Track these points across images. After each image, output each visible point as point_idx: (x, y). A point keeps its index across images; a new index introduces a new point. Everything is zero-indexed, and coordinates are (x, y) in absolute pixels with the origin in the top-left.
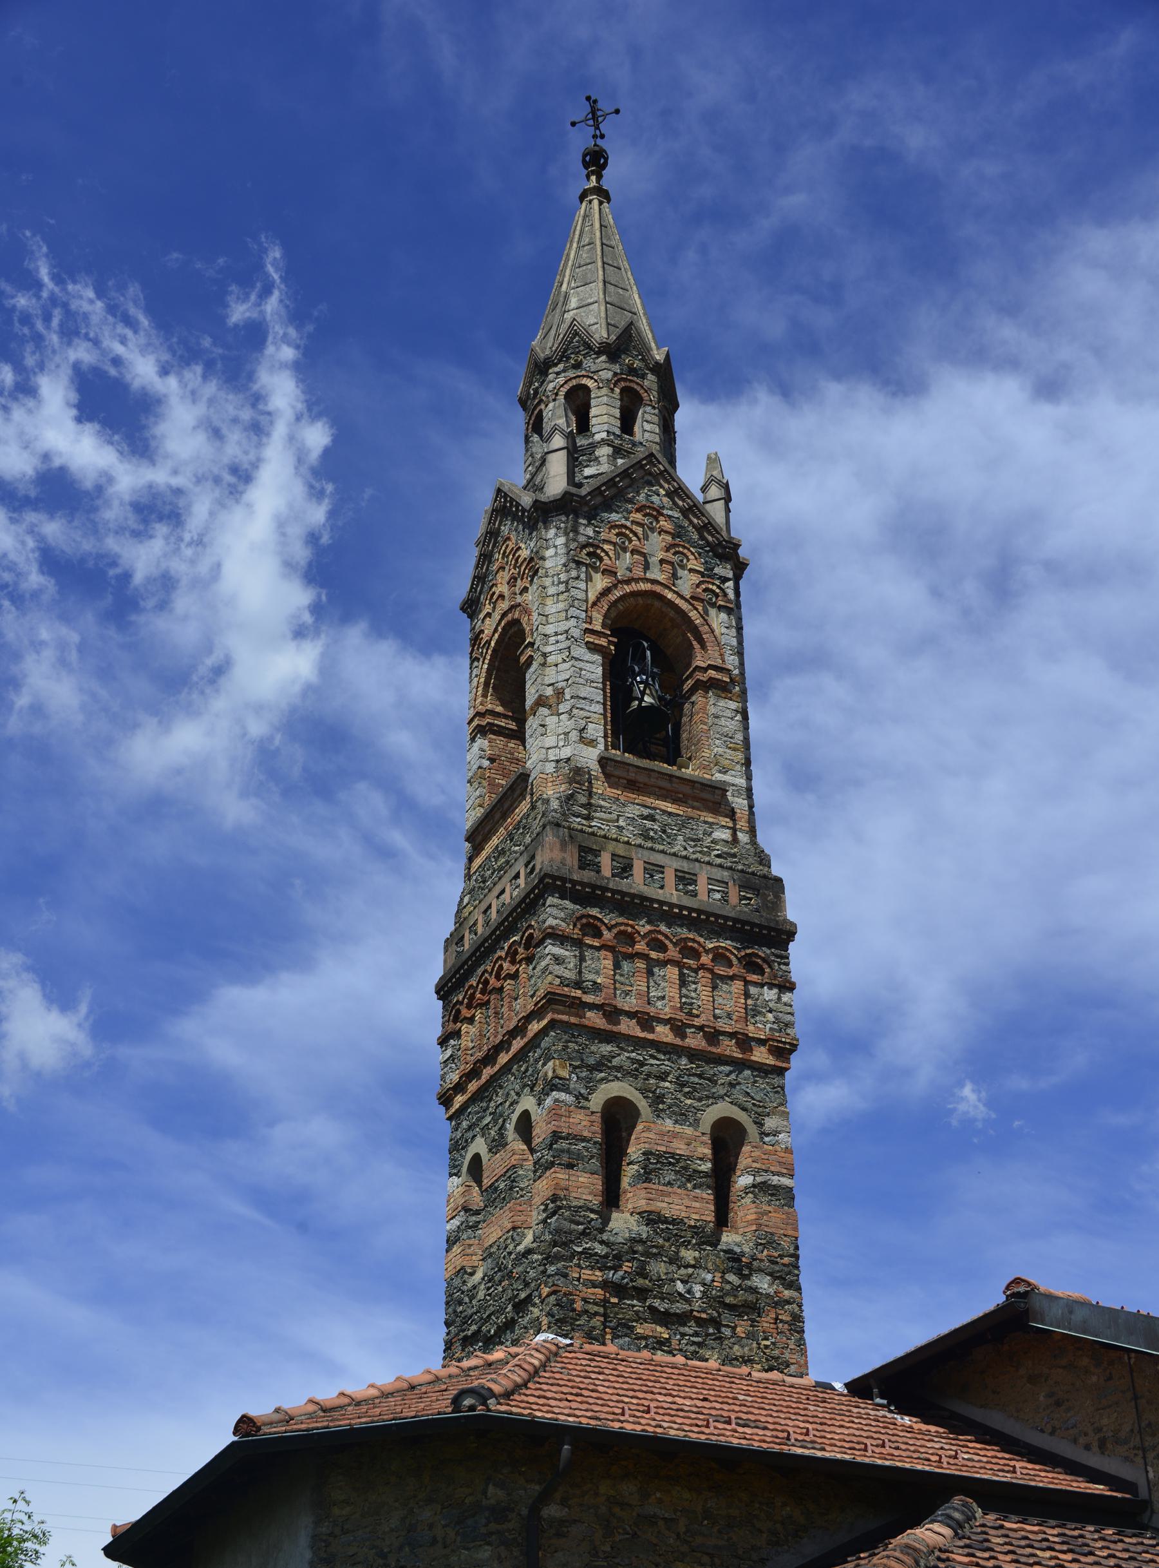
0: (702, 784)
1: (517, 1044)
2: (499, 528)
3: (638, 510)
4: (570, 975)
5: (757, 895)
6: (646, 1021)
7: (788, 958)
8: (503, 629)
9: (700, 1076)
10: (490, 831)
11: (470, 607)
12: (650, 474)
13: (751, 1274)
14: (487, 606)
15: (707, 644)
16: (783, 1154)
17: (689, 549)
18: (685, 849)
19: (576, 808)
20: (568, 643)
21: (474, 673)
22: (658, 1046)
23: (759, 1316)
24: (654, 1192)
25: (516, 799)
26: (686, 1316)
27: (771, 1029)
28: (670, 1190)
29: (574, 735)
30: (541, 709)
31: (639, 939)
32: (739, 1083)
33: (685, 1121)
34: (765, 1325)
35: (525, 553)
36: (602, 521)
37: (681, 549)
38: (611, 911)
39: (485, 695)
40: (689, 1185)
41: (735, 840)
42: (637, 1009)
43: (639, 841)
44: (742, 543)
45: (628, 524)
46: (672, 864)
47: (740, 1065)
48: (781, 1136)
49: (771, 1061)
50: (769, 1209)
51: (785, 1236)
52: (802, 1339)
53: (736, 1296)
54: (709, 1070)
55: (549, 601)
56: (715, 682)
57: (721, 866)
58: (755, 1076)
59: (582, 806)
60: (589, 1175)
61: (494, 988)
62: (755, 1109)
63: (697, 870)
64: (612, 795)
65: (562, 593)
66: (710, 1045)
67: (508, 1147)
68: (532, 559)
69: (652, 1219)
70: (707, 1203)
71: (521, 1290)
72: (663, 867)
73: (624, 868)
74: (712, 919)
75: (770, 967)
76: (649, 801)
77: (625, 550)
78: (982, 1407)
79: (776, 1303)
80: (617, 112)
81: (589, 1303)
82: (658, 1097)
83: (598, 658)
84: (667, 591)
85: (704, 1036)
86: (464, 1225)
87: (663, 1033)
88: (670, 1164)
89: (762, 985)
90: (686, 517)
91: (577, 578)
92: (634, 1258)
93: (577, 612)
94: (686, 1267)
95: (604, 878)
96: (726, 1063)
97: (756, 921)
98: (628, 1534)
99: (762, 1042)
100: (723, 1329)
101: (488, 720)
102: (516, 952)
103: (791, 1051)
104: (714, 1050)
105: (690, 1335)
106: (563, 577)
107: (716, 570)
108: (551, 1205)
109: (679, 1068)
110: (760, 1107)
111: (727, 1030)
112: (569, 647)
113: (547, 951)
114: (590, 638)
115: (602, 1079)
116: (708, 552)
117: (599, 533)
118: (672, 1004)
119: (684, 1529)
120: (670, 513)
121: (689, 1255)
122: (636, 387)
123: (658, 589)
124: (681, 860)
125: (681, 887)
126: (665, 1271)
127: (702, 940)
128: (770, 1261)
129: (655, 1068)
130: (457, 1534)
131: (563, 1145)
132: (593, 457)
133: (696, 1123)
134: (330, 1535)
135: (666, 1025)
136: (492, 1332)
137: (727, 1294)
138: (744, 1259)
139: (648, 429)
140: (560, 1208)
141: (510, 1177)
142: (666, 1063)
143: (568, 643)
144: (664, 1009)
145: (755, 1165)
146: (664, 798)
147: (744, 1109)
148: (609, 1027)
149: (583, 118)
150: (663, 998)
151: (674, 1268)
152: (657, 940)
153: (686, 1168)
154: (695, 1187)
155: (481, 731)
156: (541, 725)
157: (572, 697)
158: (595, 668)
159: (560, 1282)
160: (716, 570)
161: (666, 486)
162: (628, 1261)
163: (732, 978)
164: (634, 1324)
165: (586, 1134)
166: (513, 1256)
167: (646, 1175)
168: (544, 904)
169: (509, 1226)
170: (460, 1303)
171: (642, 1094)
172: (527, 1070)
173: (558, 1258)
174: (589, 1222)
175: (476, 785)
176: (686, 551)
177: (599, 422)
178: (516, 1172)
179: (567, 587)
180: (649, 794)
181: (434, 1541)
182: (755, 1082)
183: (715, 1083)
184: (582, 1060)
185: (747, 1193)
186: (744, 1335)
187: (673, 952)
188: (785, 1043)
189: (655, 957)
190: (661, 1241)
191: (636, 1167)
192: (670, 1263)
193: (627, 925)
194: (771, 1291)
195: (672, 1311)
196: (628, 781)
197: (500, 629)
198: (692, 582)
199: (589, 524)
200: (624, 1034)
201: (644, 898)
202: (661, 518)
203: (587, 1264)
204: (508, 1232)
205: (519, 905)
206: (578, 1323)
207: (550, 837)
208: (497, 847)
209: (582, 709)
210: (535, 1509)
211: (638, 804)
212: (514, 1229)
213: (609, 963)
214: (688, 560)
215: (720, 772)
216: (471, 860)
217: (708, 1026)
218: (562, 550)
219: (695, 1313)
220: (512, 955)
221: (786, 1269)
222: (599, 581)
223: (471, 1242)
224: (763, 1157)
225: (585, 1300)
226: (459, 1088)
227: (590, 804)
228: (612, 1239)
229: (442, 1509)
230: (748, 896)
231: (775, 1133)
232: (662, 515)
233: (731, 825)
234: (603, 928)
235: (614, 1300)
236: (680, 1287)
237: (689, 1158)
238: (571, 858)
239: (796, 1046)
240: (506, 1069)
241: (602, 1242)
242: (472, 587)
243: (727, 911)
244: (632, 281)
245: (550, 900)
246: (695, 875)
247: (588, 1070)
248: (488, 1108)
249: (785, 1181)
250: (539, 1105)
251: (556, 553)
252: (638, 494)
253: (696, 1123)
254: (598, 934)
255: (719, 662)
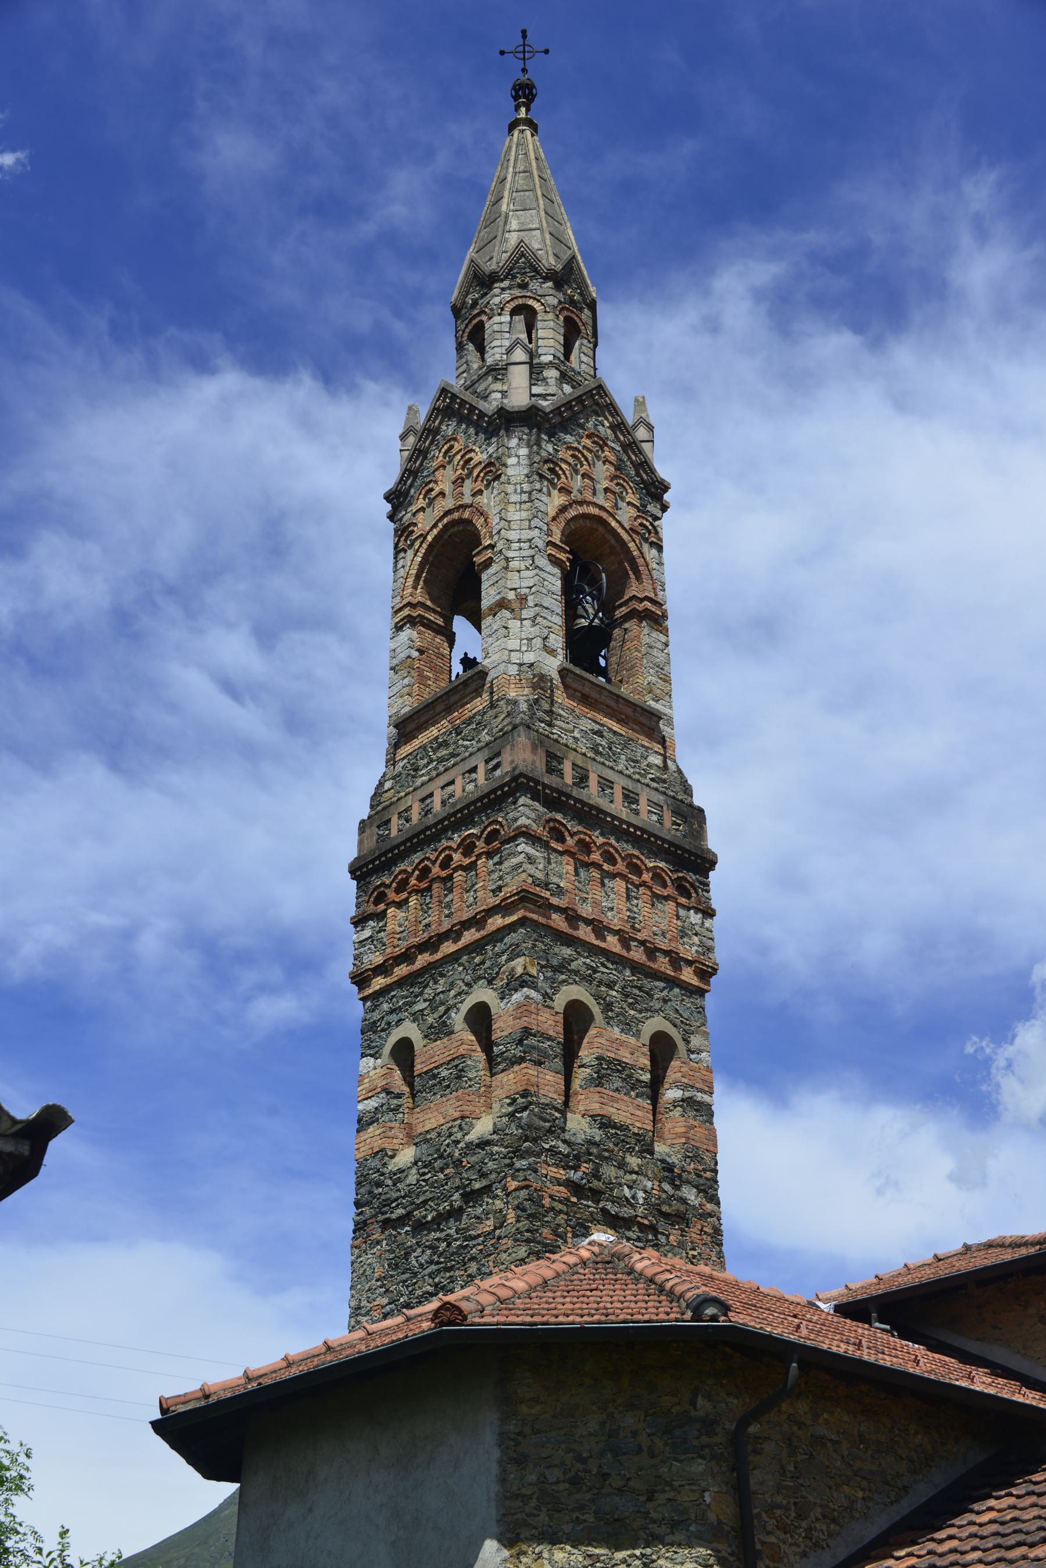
0: (643, 709)
1: (470, 936)
2: (439, 427)
3: (589, 437)
4: (540, 875)
5: (685, 822)
6: (600, 929)
7: (708, 886)
8: (445, 526)
9: (640, 989)
10: (426, 722)
11: (397, 498)
12: (597, 404)
13: (681, 1186)
14: (421, 500)
15: (643, 576)
16: (705, 1073)
17: (628, 483)
18: (627, 769)
19: (540, 714)
20: (532, 552)
21: (400, 565)
22: (606, 953)
23: (687, 1227)
24: (605, 1096)
25: (468, 695)
26: (631, 1221)
27: (697, 951)
28: (618, 1096)
29: (538, 643)
30: (504, 611)
31: (594, 849)
32: (670, 1000)
33: (630, 1030)
34: (693, 1235)
35: (480, 456)
36: (560, 441)
37: (622, 482)
38: (572, 819)
39: (415, 587)
40: (632, 1093)
41: (665, 767)
42: (594, 916)
43: (590, 754)
44: (672, 486)
45: (581, 448)
46: (620, 782)
47: (673, 982)
48: (704, 1054)
49: (695, 981)
50: (696, 1123)
51: (708, 1151)
52: (721, 1251)
53: (670, 1206)
54: (648, 984)
55: (511, 508)
56: (650, 613)
57: (656, 789)
58: (682, 995)
59: (545, 712)
60: (554, 1074)
61: (438, 877)
62: (682, 1026)
63: (638, 791)
64: (569, 706)
65: (525, 502)
66: (649, 960)
67: (453, 1036)
68: (490, 464)
69: (605, 1123)
70: (647, 1112)
71: (475, 1180)
72: (613, 783)
73: (582, 780)
74: (652, 839)
75: (696, 892)
76: (599, 717)
77: (576, 472)
78: (978, 1340)
79: (700, 1215)
80: (502, 53)
81: (555, 1200)
82: (608, 1005)
83: (557, 571)
84: (611, 519)
85: (645, 950)
86: (385, 1108)
87: (612, 943)
88: (618, 1071)
89: (689, 909)
90: (626, 452)
91: (540, 491)
92: (590, 1160)
93: (540, 524)
94: (631, 1172)
95: (567, 785)
96: (660, 979)
97: (687, 847)
98: (806, 1454)
99: (689, 963)
100: (659, 1236)
101: (419, 612)
102: (473, 845)
103: (712, 975)
104: (652, 965)
105: (634, 1240)
106: (526, 487)
107: (649, 508)
108: (520, 1100)
109: (624, 979)
110: (687, 1025)
111: (663, 947)
112: (533, 556)
113: (520, 849)
114: (551, 551)
115: (564, 981)
116: (642, 489)
117: (558, 451)
118: (621, 916)
119: (846, 1453)
120: (613, 445)
121: (633, 1161)
122: (576, 318)
123: (604, 515)
124: (627, 778)
125: (626, 804)
126: (615, 1175)
127: (643, 858)
128: (696, 1174)
129: (605, 977)
130: (666, 1444)
131: (532, 1041)
132: (541, 377)
133: (638, 1034)
134: (520, 1433)
135: (614, 936)
136: (429, 1218)
137: (663, 1203)
138: (676, 1170)
139: (585, 361)
140: (531, 1103)
141: (457, 1066)
142: (614, 972)
143: (532, 552)
144: (613, 919)
145: (684, 1080)
146: (610, 716)
147: (675, 1026)
148: (570, 931)
149: (512, 49)
150: (611, 909)
151: (621, 1173)
152: (609, 852)
153: (630, 1076)
154: (637, 1096)
155: (412, 621)
156: (504, 627)
157: (536, 605)
158: (556, 584)
159: (532, 1177)
160: (649, 508)
161: (611, 419)
162: (585, 1162)
163: (667, 898)
164: (590, 1224)
165: (551, 1033)
166: (462, 1145)
167: (598, 1080)
168: (514, 803)
169: (457, 1114)
170: (379, 1184)
171: (596, 999)
172: (483, 963)
173: (529, 1153)
174: (554, 1120)
175: (404, 673)
176: (625, 484)
177: (545, 344)
178: (464, 1062)
179: (530, 498)
180: (599, 710)
181: (639, 1450)
182: (683, 1000)
183: (651, 996)
184: (548, 961)
185: (675, 1107)
186: (675, 1244)
187: (621, 866)
188: (708, 966)
189: (606, 869)
190: (611, 1145)
191: (588, 1070)
192: (619, 1168)
193: (586, 834)
194: (696, 1203)
195: (621, 1215)
196: (583, 695)
197: (440, 525)
198: (630, 515)
199: (549, 441)
200: (581, 940)
201: (600, 811)
202: (606, 448)
203: (553, 1161)
204: (455, 1120)
205: (480, 799)
206: (546, 1219)
207: (522, 739)
208: (437, 738)
209: (545, 618)
210: (744, 1423)
211: (590, 719)
212: (463, 1118)
213: (571, 868)
214: (627, 493)
215: (653, 700)
216: (396, 746)
217: (650, 942)
218: (525, 461)
219: (639, 1219)
220: (467, 848)
221: (709, 1183)
222: (556, 498)
223: (392, 1125)
224: (691, 1073)
225: (551, 1196)
226: (382, 969)
227: (551, 711)
228: (573, 1139)
229: (646, 1416)
230: (678, 821)
231: (699, 1052)
232: (607, 445)
233: (662, 751)
234: (566, 834)
235: (574, 1199)
236: (627, 1192)
237: (633, 1067)
238: (540, 765)
239: (715, 970)
240: (453, 958)
241: (565, 1141)
242: (401, 479)
243: (663, 834)
244: (566, 218)
245: (522, 800)
246: (637, 795)
247: (552, 971)
248: (421, 994)
249: (706, 1098)
250: (502, 999)
251: (519, 462)
252: (588, 422)
253: (638, 1034)
254: (561, 840)
255: (652, 595)
